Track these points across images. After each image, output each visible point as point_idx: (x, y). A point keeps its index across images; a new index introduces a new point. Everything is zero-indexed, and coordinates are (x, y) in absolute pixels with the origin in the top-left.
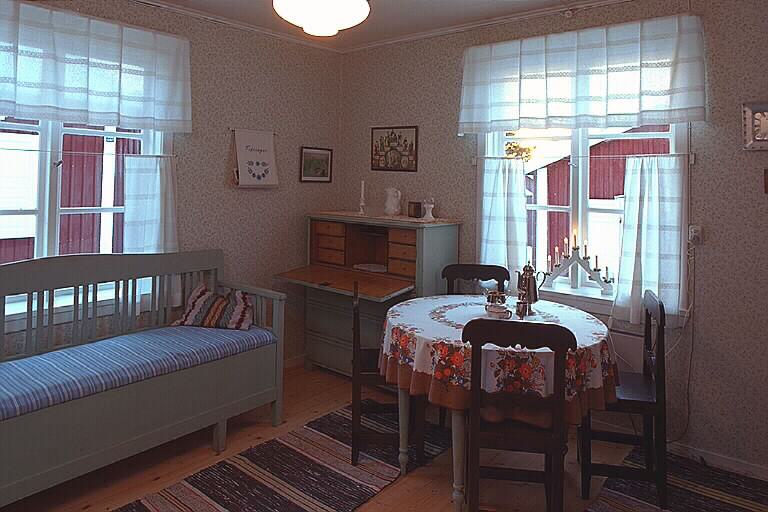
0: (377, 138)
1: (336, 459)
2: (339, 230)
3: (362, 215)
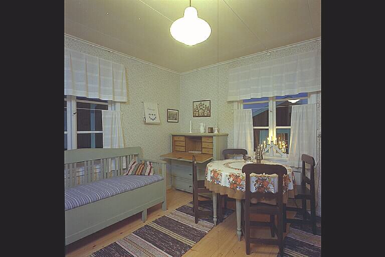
0: (195, 105)
1: (188, 220)
2: (183, 139)
3: (191, 133)
